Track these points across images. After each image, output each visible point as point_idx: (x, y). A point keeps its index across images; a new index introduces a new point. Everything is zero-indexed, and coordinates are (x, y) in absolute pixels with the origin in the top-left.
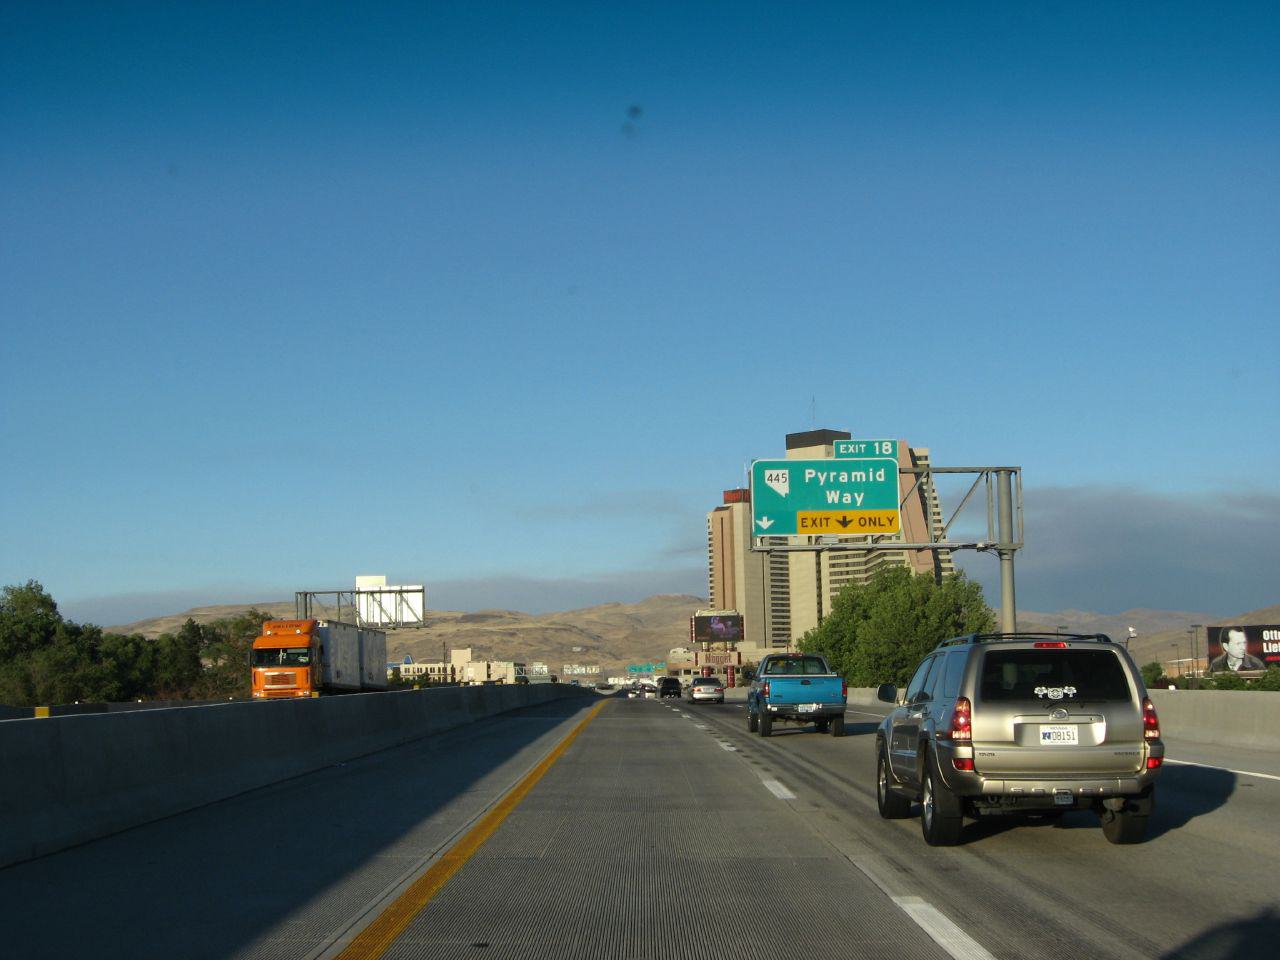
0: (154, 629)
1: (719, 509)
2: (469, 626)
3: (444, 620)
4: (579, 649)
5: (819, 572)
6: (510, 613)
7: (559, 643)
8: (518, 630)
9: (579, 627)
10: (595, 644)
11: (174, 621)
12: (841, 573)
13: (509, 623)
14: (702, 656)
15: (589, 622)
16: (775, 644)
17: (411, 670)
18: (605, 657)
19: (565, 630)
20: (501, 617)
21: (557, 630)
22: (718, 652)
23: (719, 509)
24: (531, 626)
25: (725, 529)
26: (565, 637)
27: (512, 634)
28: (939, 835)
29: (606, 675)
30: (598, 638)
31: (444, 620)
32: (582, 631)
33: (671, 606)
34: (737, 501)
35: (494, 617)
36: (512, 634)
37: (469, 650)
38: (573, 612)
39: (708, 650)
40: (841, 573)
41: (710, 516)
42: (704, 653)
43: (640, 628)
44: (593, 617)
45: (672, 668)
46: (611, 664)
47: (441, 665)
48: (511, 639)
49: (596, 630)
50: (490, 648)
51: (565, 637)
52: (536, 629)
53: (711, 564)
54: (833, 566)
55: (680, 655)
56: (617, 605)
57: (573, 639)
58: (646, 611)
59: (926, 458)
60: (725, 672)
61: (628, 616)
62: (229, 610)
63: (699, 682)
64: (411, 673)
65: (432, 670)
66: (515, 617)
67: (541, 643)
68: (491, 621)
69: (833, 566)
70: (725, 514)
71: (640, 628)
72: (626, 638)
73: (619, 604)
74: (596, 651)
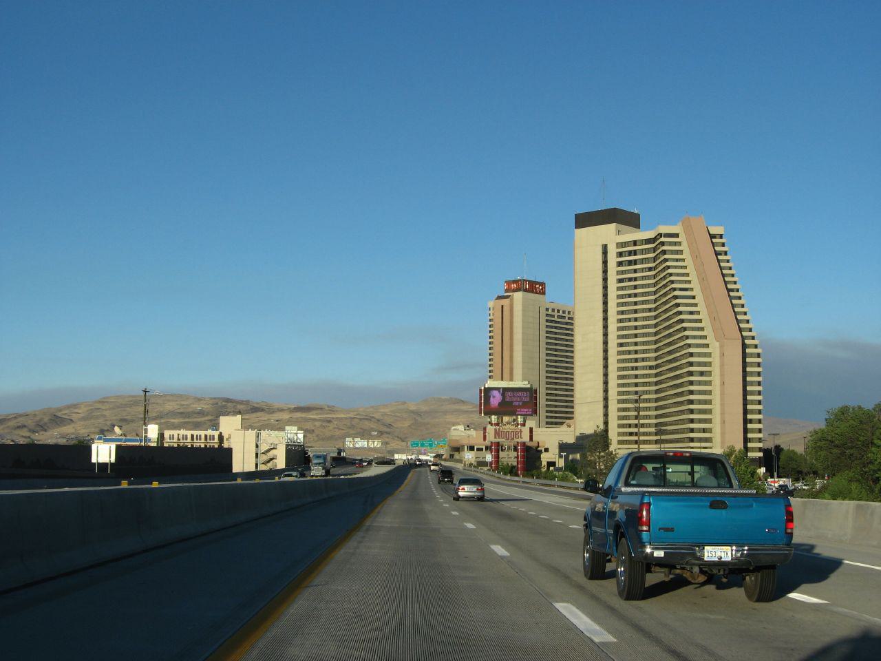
0: (76, 411)
1: (499, 298)
2: (299, 415)
3: (281, 410)
4: (376, 433)
5: (606, 351)
6: (328, 407)
7: (361, 428)
8: (333, 418)
9: (377, 417)
10: (388, 430)
11: (91, 405)
12: (629, 352)
13: (328, 413)
14: (491, 430)
15: (385, 414)
16: (547, 426)
17: (176, 437)
18: (394, 439)
19: (367, 419)
20: (321, 409)
21: (361, 419)
22: (508, 426)
23: (499, 298)
24: (343, 416)
25: (504, 316)
26: (367, 425)
27: (329, 421)
28: (636, 591)
29: (392, 452)
30: (390, 426)
31: (281, 410)
32: (378, 420)
33: (442, 405)
34: (518, 290)
35: (317, 409)
36: (329, 421)
37: (239, 417)
38: (373, 407)
39: (497, 424)
40: (629, 352)
41: (491, 304)
42: (493, 427)
43: (419, 419)
44: (387, 410)
45: (456, 445)
46: (395, 444)
47: (210, 432)
48: (328, 424)
49: (388, 420)
50: (313, 430)
51: (367, 425)
52: (346, 418)
53: (490, 349)
54: (621, 345)
55: (459, 432)
56: (404, 403)
57: (372, 426)
58: (424, 408)
59: (721, 236)
60: (516, 449)
61: (413, 412)
62: (131, 399)
63: (433, 465)
64: (175, 440)
65: (199, 437)
66: (331, 410)
67: (350, 428)
68: (315, 412)
69: (621, 345)
70: (506, 302)
71: (419, 419)
72: (409, 426)
73: (405, 403)
74: (388, 435)
